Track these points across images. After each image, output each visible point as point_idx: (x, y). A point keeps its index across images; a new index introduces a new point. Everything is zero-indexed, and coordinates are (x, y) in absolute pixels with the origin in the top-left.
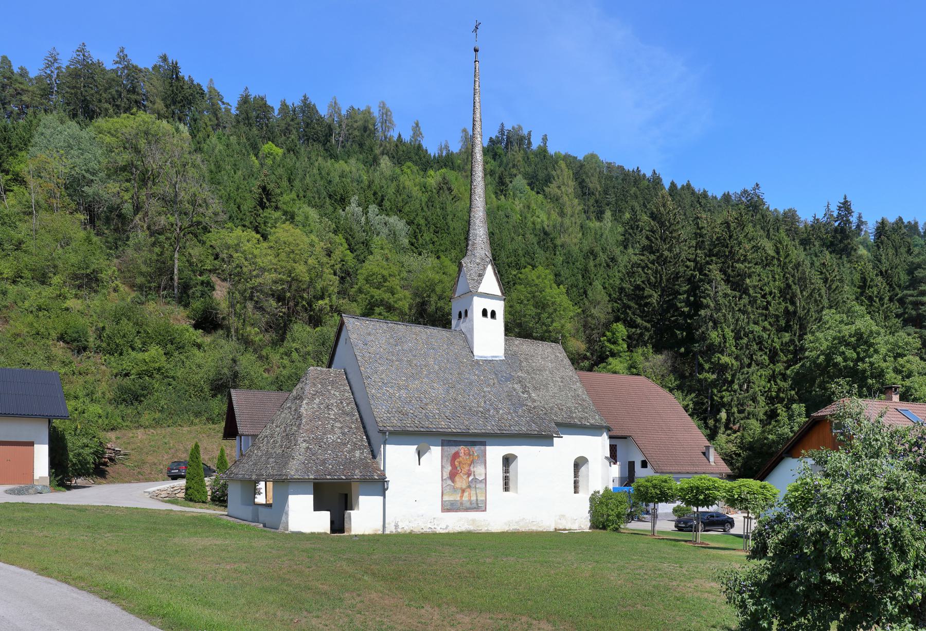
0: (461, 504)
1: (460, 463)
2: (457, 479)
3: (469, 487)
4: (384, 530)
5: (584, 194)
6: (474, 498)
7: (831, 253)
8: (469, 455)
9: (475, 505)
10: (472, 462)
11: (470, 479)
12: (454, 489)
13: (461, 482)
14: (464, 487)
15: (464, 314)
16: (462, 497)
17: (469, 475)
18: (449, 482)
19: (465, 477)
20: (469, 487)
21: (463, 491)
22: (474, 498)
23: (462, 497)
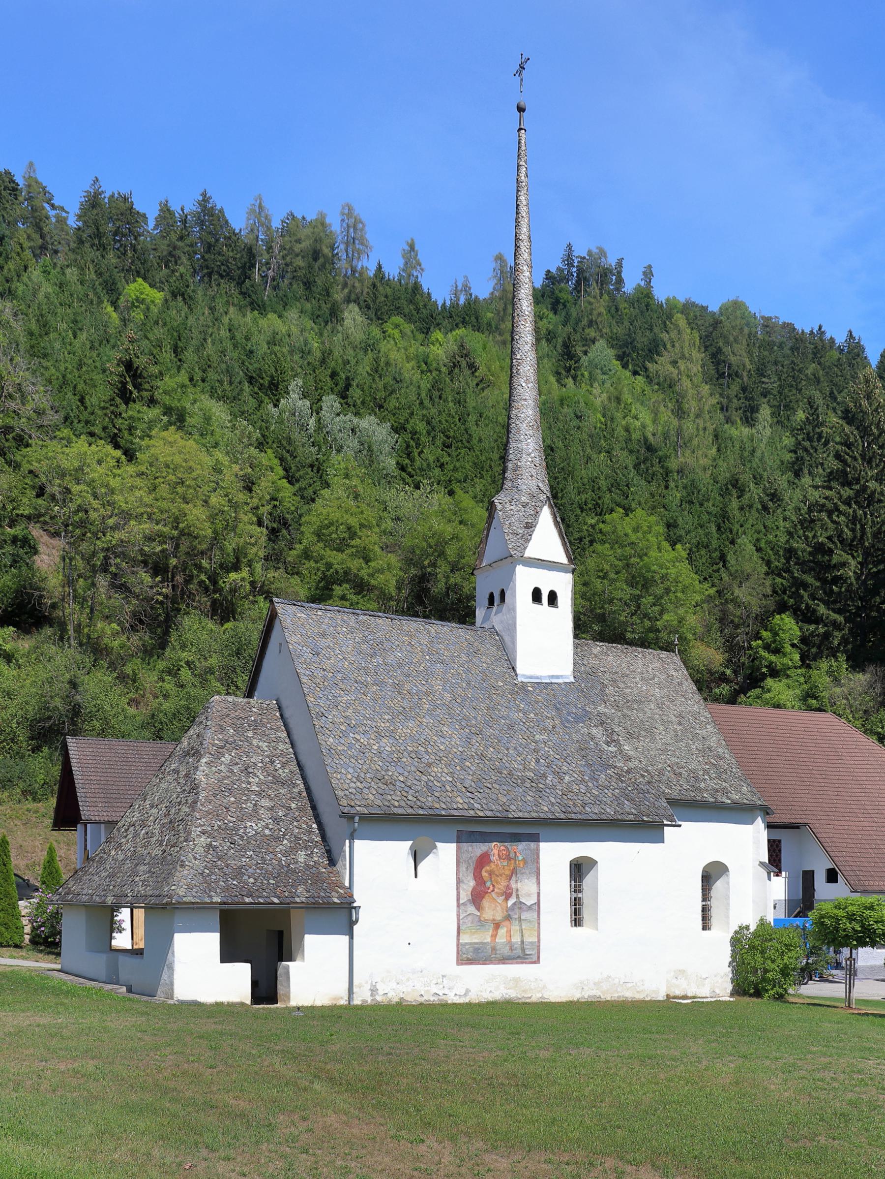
1: (491, 873)
2: (485, 903)
3: (508, 918)
6: (516, 939)
9: (519, 952)
10: (514, 872)
11: (510, 903)
12: (481, 923)
13: (493, 909)
14: (499, 917)
15: (499, 598)
16: (494, 936)
17: (508, 896)
18: (471, 909)
19: (500, 899)
20: (508, 918)
21: (497, 926)
22: (516, 939)
23: (494, 936)
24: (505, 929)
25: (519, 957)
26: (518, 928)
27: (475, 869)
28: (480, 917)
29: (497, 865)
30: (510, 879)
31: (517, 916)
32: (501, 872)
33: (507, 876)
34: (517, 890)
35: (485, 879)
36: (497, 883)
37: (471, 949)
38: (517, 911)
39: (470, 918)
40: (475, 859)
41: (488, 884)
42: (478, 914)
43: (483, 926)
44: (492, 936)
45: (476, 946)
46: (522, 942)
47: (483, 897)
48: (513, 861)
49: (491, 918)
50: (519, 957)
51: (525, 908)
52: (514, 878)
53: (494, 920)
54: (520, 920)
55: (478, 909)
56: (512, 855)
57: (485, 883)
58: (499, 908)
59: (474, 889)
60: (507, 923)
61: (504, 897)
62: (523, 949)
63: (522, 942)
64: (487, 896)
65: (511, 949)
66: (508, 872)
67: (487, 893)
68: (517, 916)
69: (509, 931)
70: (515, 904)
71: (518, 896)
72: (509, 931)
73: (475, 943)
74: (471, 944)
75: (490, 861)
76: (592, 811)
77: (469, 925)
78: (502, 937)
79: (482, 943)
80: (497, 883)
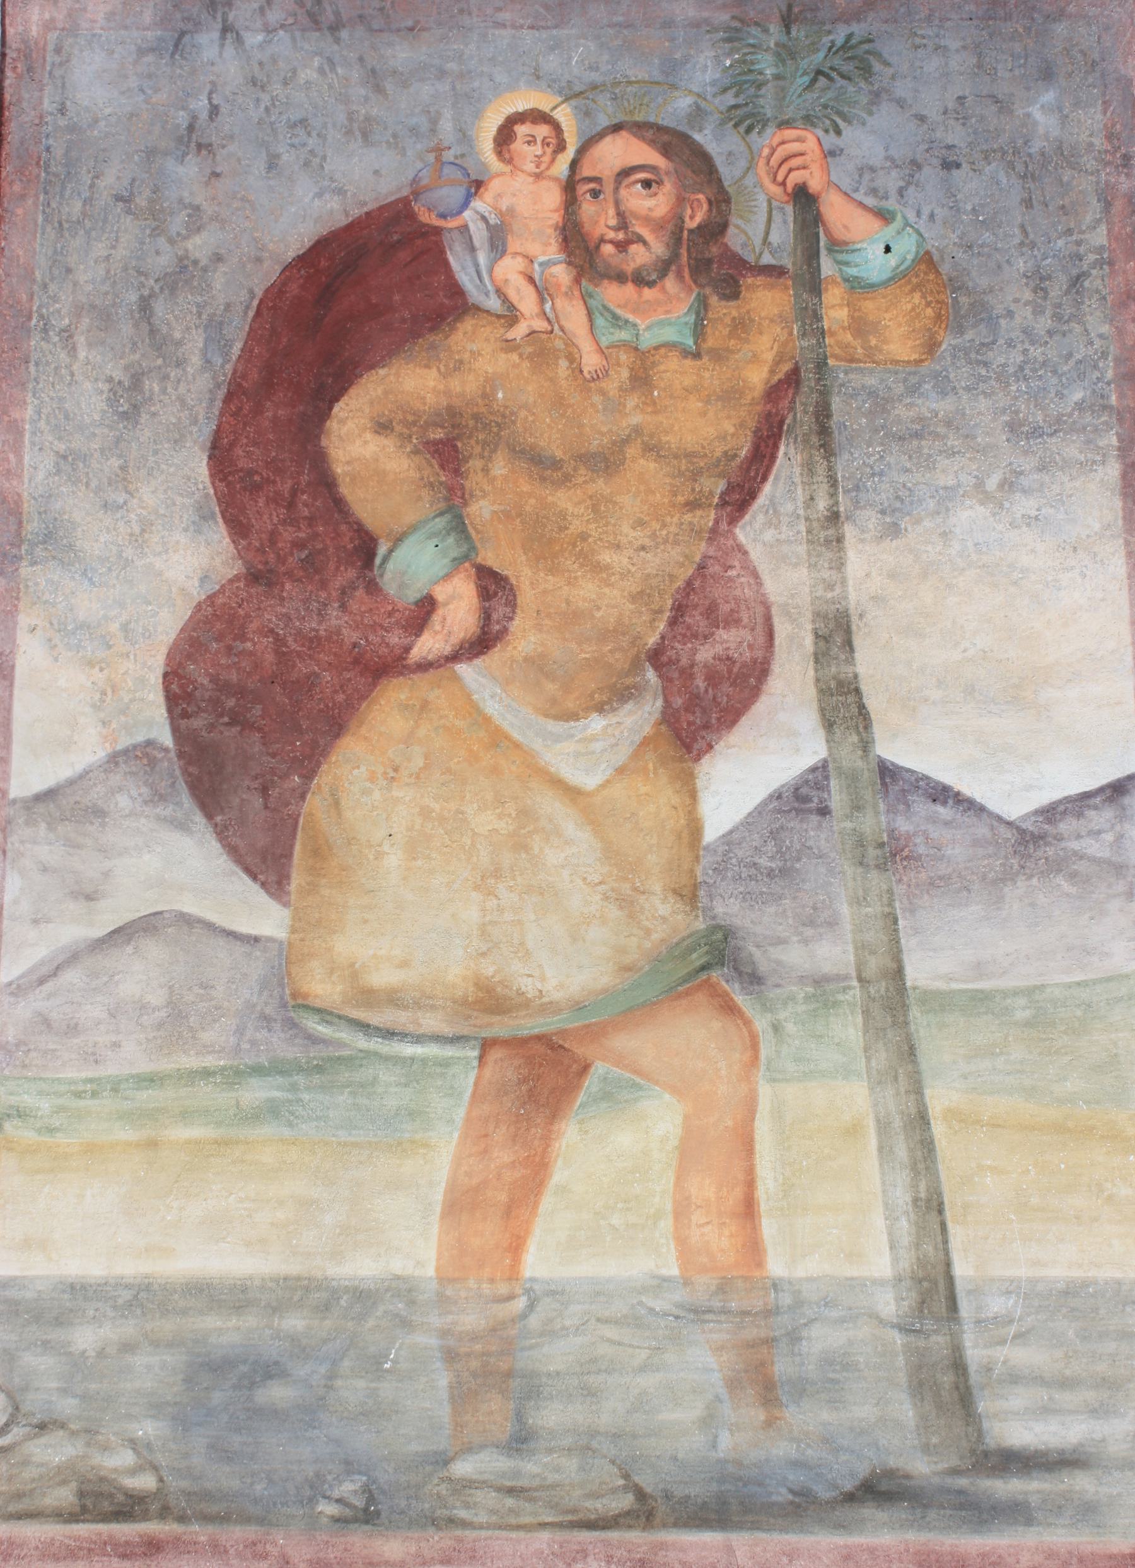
0: (494, 1373)
1: (446, 448)
2: (376, 783)
3: (712, 967)
4: (561, 262)
5: (143, 1007)
6: (837, 1239)
7: (90, 345)
8: (709, 261)
9: (885, 1423)
10: (790, 415)
11: (740, 780)
12: (304, 1042)
13: (484, 840)
14: (562, 965)
15: (719, 1461)
16: (499, 1203)
17: (701, 708)
18: (178, 863)
19: (596, 748)
20: (712, 967)
21: (541, 1070)
22: (837, 1239)
23: (499, 1203)
24: (661, 1120)
25: (879, 1490)
26: (856, 1098)
27: (241, 399)
28: (285, 961)
29: (542, 349)
30: (740, 498)
31: (834, 954)
32: (598, 427)
33: (691, 465)
34: (836, 634)
35: (368, 505)
36: (547, 542)
37: (151, 1371)
38: (841, 889)
39: (141, 975)
40: (236, 289)
41: (417, 564)
42: (267, 918)
43: (325, 1066)
44: (461, 1204)
45: (225, 1331)
46: (935, 1292)
47: (336, 723)
48: (767, 302)
49: (455, 968)
50: (879, 1490)
51: (954, 844)
52: (786, 484)
53: (491, 999)
54: (890, 999)
55: (267, 859)
56: (761, 230)
57: (364, 549)
58: (571, 853)
59: (214, 626)
60: (691, 1037)
61: (640, 717)
62: (951, 1392)
63: (935, 1292)
64: (389, 712)
65: (761, 1380)
66: (711, 427)
67: (385, 667)
68: (834, 954)
69: (726, 1155)
70: (803, 798)
71: (844, 706)
72: (726, 1155)
73: (205, 1293)
74: (144, 1298)
75: (448, 306)
76: (221, 941)
77: (133, 1056)
78: (613, 1202)
79: (295, 1292)
80: (547, 542)
